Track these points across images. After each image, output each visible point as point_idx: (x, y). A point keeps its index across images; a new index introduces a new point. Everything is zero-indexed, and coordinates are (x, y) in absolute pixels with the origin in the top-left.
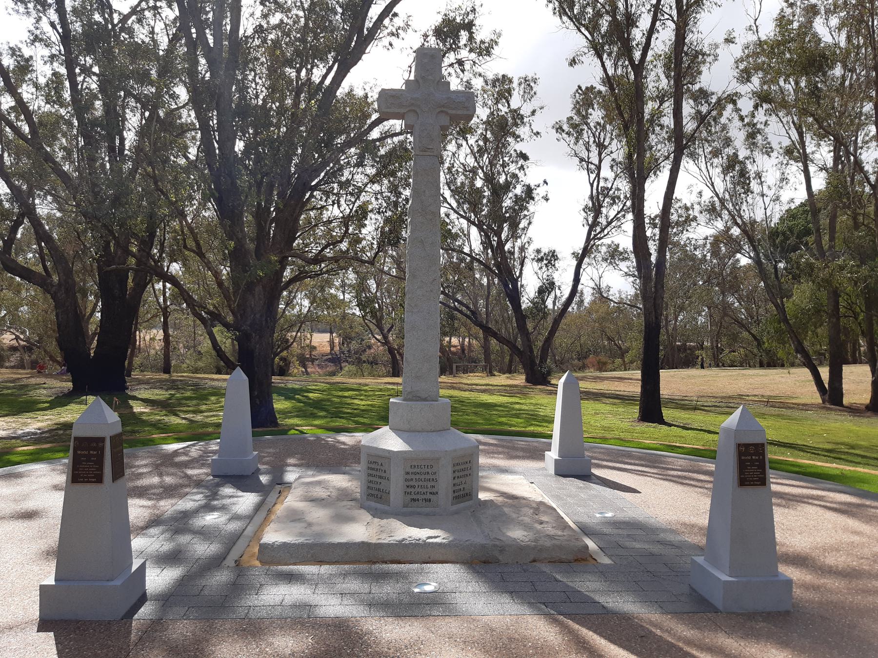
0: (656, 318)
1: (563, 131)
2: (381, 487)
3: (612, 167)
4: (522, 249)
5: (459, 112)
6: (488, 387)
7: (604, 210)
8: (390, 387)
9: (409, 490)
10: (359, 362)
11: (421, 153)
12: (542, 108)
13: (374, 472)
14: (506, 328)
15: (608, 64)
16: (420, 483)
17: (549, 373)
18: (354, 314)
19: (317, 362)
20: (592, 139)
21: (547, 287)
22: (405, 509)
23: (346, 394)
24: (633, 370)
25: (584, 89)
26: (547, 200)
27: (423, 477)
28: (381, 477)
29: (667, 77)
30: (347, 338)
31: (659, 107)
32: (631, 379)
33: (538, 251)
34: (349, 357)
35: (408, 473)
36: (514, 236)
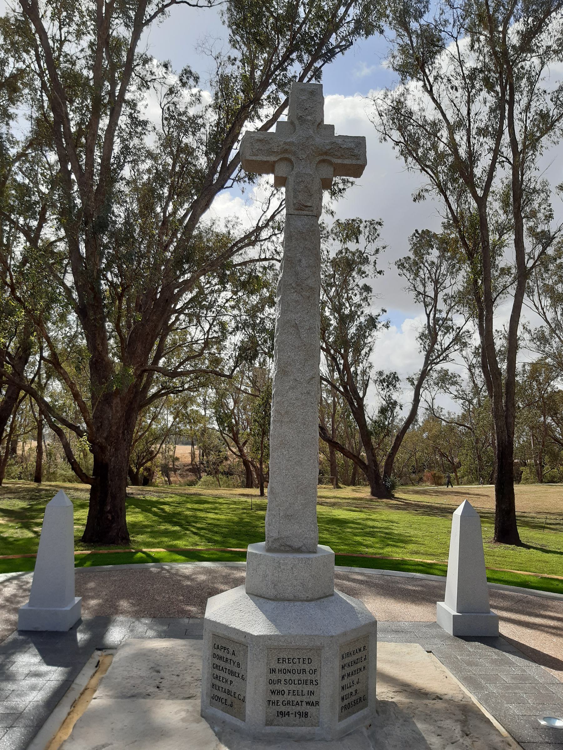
0: (509, 436)
1: (404, 267)
2: (233, 689)
3: (445, 301)
4: (364, 372)
5: (347, 162)
6: (336, 500)
7: (439, 338)
8: (243, 499)
9: (275, 698)
10: (214, 472)
11: (296, 212)
12: (384, 248)
13: (222, 664)
14: (349, 443)
15: (451, 199)
16: (292, 687)
17: (393, 487)
18: (213, 429)
19: (179, 472)
20: (427, 275)
21: (389, 407)
22: (268, 729)
23: (202, 506)
24: (465, 484)
25: (420, 232)
26: (388, 327)
27: (296, 677)
28: (232, 673)
29: (505, 212)
30: (206, 451)
31: (499, 239)
32: (468, 494)
33: (381, 373)
34: (208, 467)
35: (273, 671)
36: (357, 362)
